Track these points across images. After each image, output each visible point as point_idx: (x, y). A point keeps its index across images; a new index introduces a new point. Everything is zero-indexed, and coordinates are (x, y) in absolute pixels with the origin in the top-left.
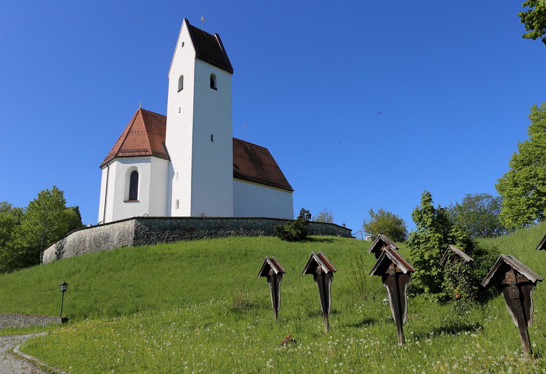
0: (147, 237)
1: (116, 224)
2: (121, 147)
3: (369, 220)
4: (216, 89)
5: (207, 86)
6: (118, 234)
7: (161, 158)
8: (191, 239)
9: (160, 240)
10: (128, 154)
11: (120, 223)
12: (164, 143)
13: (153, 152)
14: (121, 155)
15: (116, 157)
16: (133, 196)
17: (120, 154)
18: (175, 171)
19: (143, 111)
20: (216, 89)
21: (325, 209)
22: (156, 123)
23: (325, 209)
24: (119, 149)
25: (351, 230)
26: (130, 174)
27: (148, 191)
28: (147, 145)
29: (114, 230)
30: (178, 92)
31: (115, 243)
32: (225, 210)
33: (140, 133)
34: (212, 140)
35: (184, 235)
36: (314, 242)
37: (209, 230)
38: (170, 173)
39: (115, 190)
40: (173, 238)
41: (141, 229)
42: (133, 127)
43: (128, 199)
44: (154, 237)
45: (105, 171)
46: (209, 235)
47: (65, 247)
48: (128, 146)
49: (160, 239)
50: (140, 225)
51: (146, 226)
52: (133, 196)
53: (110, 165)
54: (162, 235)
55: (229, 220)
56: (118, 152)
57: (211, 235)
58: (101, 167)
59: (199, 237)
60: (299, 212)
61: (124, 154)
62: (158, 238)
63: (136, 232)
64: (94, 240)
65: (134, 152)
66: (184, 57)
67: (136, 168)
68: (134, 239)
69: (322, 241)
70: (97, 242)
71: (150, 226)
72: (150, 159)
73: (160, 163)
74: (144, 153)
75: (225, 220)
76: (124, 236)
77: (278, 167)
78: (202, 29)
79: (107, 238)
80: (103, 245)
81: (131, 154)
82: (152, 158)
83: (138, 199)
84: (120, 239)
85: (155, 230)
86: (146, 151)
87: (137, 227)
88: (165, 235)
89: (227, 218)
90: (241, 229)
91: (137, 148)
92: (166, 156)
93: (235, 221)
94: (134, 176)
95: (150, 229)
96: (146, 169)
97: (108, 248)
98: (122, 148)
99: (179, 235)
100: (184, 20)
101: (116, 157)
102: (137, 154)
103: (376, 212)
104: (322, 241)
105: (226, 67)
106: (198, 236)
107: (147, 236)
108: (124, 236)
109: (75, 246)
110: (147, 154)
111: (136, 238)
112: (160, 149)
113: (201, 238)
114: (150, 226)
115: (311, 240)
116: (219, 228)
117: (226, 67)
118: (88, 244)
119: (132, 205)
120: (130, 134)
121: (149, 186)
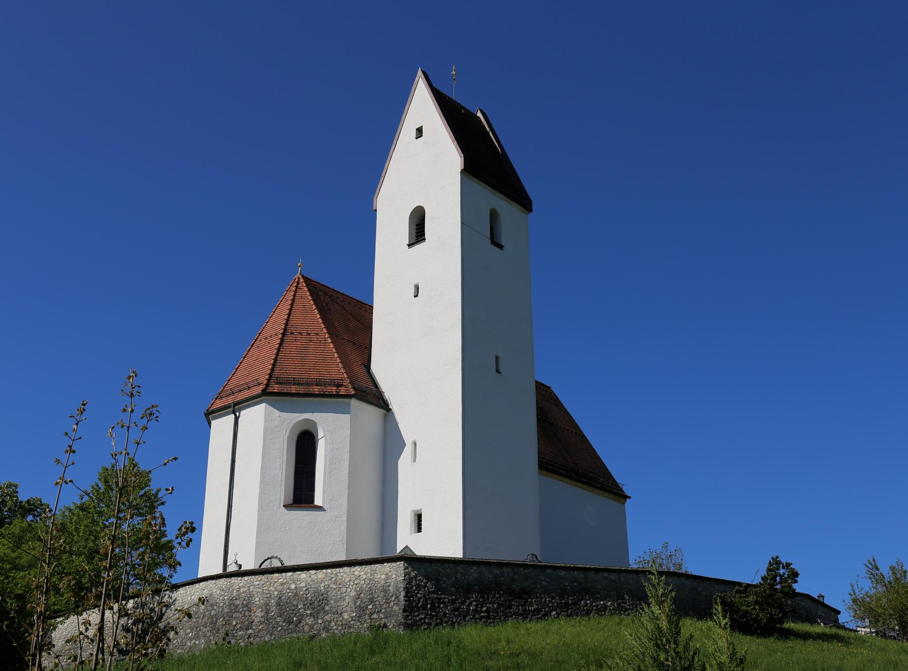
0: (433, 608)
1: (346, 569)
2: (272, 370)
3: (866, 587)
4: (501, 247)
5: (484, 240)
6: (353, 593)
7: (371, 403)
8: (525, 615)
9: (459, 615)
10: (294, 389)
11: (358, 568)
12: (368, 366)
13: (354, 388)
14: (278, 390)
15: (266, 394)
16: (302, 495)
17: (276, 388)
18: (408, 439)
19: (309, 282)
20: (501, 247)
21: (665, 546)
22: (348, 319)
23: (665, 546)
24: (271, 375)
25: (839, 613)
26: (296, 438)
27: (345, 484)
28: (337, 371)
29: (340, 585)
30: (410, 245)
31: (346, 616)
32: (519, 545)
33: (315, 338)
34: (498, 371)
35: (510, 607)
36: (810, 642)
37: (561, 596)
38: (390, 443)
39: (263, 475)
40: (487, 611)
41: (418, 586)
42: (291, 323)
43: (291, 502)
44: (446, 607)
45: (221, 427)
46: (561, 608)
47: (171, 617)
48: (291, 368)
49: (460, 617)
50: (415, 577)
51: (429, 580)
52: (302, 495)
53: (240, 410)
54: (463, 603)
55: (600, 574)
56: (269, 380)
57: (569, 610)
58: (211, 414)
59: (541, 614)
60: (767, 564)
61: (285, 389)
62: (455, 610)
63: (407, 590)
64: (278, 604)
65: (308, 384)
66: (424, 165)
67: (314, 424)
68: (404, 611)
69: (805, 636)
70: (288, 611)
71: (437, 580)
72: (349, 404)
73: (369, 413)
74: (333, 390)
75: (592, 575)
76: (371, 600)
77: (584, 436)
78: (453, 97)
79: (319, 603)
80: (310, 621)
81: (302, 389)
82: (354, 402)
83: (318, 501)
84: (361, 609)
85: (437, 588)
86: (339, 386)
87: (409, 581)
88: (470, 604)
89: (596, 570)
90: (627, 597)
91: (314, 375)
92: (375, 397)
93: (613, 577)
94: (305, 446)
95: (438, 589)
96: (335, 431)
97: (327, 629)
98: (276, 373)
99: (500, 605)
100: (420, 73)
101: (265, 393)
102: (316, 389)
103: (885, 571)
104: (805, 636)
105: (523, 200)
106: (538, 610)
107: (433, 604)
108: (371, 600)
109: (216, 617)
110: (343, 391)
111: (409, 609)
112: (365, 384)
113: (546, 615)
114: (437, 580)
115: (787, 634)
116: (582, 591)
117: (523, 200)
118: (258, 614)
119: (302, 516)
120: (289, 338)
121: (347, 471)
